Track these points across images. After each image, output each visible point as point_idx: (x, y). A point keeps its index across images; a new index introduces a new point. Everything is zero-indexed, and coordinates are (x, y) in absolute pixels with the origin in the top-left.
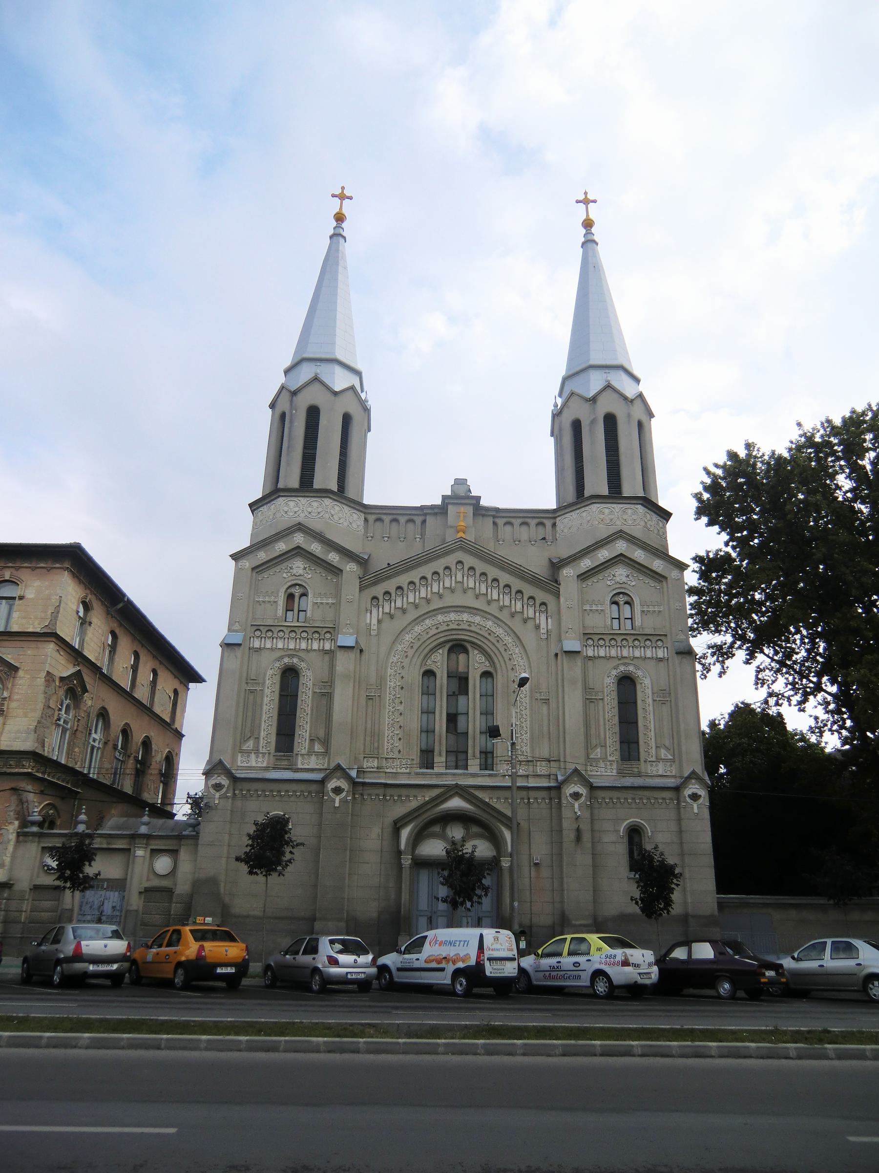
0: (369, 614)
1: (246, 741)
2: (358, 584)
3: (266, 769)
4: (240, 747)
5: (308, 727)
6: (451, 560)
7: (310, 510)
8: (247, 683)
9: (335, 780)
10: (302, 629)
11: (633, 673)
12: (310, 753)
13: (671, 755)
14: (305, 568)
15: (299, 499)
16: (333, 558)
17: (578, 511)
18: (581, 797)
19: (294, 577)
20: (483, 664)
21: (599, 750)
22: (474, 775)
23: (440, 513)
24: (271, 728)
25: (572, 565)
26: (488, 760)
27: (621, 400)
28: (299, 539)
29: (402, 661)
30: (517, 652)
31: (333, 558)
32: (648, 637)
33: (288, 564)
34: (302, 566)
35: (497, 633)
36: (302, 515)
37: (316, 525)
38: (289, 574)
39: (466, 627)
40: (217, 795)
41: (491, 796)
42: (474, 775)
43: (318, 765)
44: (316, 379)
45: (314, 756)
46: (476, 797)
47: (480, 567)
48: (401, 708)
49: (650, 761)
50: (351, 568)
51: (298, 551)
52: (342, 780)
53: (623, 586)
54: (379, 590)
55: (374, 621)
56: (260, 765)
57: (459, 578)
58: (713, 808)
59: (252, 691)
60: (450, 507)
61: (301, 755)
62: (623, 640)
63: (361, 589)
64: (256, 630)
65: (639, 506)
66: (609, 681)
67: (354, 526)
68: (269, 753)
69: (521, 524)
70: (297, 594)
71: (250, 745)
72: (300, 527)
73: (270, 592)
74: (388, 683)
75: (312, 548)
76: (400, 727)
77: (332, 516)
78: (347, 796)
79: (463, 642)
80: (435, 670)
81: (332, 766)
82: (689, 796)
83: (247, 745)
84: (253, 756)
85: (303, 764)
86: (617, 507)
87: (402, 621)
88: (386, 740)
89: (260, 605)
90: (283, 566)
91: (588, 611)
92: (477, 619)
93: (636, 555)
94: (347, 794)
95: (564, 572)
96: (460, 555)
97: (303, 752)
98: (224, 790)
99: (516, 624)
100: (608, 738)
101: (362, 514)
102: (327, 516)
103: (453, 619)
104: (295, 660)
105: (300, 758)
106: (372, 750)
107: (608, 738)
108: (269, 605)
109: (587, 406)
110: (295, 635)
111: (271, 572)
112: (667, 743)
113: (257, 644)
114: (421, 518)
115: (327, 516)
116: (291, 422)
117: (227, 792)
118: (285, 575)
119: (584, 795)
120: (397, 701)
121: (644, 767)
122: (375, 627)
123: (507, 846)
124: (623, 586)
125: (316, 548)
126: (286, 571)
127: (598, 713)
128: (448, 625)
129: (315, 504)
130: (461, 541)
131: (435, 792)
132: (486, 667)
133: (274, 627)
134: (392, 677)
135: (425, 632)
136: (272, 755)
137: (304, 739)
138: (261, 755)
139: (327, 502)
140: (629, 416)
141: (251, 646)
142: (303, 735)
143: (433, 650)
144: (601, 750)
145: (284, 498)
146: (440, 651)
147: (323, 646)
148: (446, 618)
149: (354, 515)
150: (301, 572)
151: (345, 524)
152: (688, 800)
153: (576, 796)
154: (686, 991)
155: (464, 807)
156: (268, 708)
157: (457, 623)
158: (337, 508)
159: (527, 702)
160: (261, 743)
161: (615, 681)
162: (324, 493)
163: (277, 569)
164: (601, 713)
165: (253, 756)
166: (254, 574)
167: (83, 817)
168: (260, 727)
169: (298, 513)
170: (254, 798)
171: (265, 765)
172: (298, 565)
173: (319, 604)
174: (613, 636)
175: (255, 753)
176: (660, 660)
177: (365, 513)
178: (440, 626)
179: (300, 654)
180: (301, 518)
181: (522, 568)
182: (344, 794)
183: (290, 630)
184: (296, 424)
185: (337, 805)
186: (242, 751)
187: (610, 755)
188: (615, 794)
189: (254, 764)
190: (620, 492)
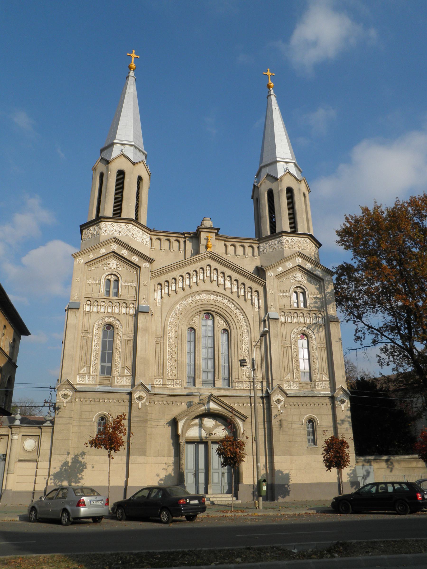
0: (156, 293)
1: (81, 368)
2: (150, 275)
4: (78, 372)
5: (120, 360)
7: (120, 230)
8: (82, 333)
9: (138, 392)
10: (116, 301)
12: (122, 375)
14: (117, 265)
15: (114, 223)
16: (135, 259)
19: (110, 270)
20: (222, 325)
21: (289, 375)
22: (219, 389)
23: (194, 237)
24: (98, 360)
25: (272, 269)
26: (229, 382)
27: (295, 180)
30: (242, 318)
33: (107, 261)
34: (115, 263)
35: (231, 307)
38: (294, 280)
39: (212, 303)
40: (65, 401)
42: (219, 389)
43: (127, 383)
46: (223, 402)
47: (221, 268)
48: (176, 349)
49: (317, 382)
51: (115, 254)
52: (142, 392)
54: (162, 279)
55: (159, 297)
58: (352, 409)
59: (85, 338)
60: (202, 233)
65: (307, 239)
67: (145, 241)
68: (97, 376)
69: (231, 245)
70: (112, 280)
71: (84, 370)
72: (117, 241)
73: (96, 278)
75: (122, 253)
77: (133, 234)
78: (146, 402)
80: (195, 328)
82: (62, 395)
83: (82, 370)
84: (87, 377)
85: (118, 383)
86: (296, 239)
87: (174, 297)
88: (167, 369)
90: (104, 263)
92: (219, 298)
93: (122, 253)
94: (146, 400)
95: (77, 260)
97: (118, 375)
101: (148, 235)
102: (130, 234)
104: (112, 319)
105: (116, 379)
106: (159, 375)
111: (96, 266)
114: (184, 240)
115: (130, 234)
116: (107, 179)
117: (71, 399)
118: (105, 268)
119: (283, 401)
120: (173, 345)
122: (160, 301)
125: (124, 253)
126: (105, 266)
128: (202, 301)
129: (123, 227)
130: (210, 253)
132: (225, 326)
133: (99, 299)
135: (189, 305)
136: (98, 376)
138: (91, 377)
139: (130, 226)
140: (299, 189)
141: (85, 310)
142: (117, 365)
143: (194, 316)
144: (290, 375)
145: (104, 223)
147: (129, 312)
149: (144, 235)
150: (115, 266)
153: (279, 401)
154: (418, 513)
155: (216, 408)
156: (95, 348)
157: (207, 300)
158: (136, 230)
162: (128, 220)
163: (100, 264)
165: (87, 377)
166: (86, 266)
169: (113, 232)
170: (87, 403)
171: (94, 383)
172: (113, 263)
175: (87, 375)
177: (150, 235)
178: (198, 302)
179: (116, 316)
180: (115, 235)
181: (244, 270)
182: (144, 400)
183: (108, 301)
186: (79, 374)
190: (120, 215)
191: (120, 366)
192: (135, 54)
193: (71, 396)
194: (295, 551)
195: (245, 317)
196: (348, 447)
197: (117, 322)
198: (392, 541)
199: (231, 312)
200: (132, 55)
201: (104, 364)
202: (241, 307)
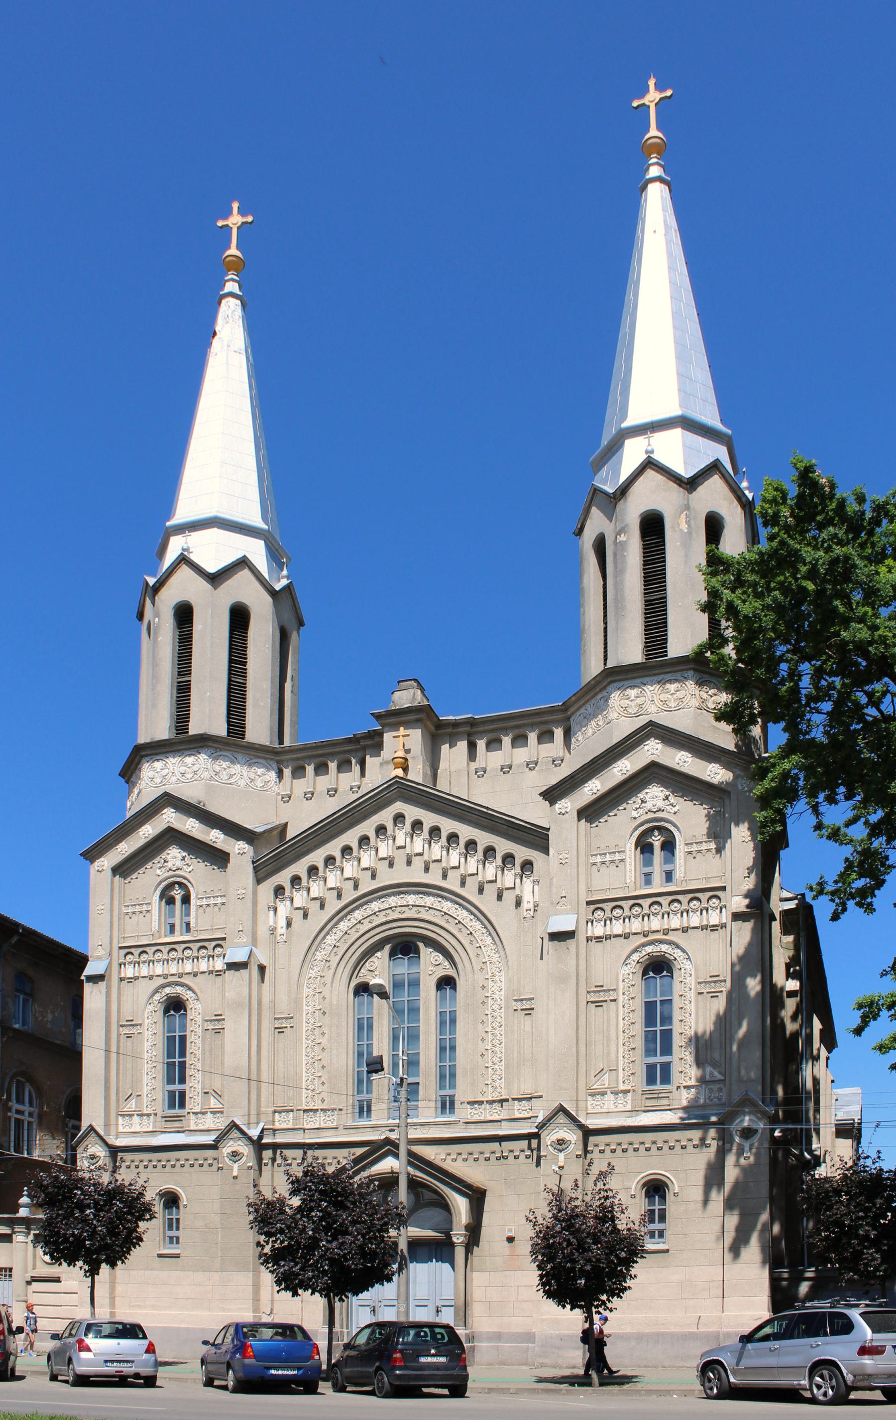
3: (634, 1111)
6: (385, 816)
11: (666, 955)
13: (720, 1073)
16: (216, 837)
17: (593, 701)
18: (753, 1135)
19: (171, 873)
21: (606, 1076)
28: (169, 817)
29: (322, 975)
31: (216, 837)
32: (694, 894)
36: (174, 779)
37: (190, 793)
41: (448, 1152)
44: (650, 464)
45: (209, 1113)
50: (238, 849)
51: (171, 836)
53: (178, 872)
54: (283, 877)
55: (282, 923)
56: (621, 1108)
57: (400, 841)
61: (193, 1113)
62: (186, 948)
63: (259, 881)
64: (186, 948)
66: (628, 971)
74: (305, 1007)
75: (187, 827)
76: (323, 1067)
79: (414, 939)
81: (736, 1098)
85: (197, 1126)
89: (694, 858)
91: (599, 864)
93: (677, 760)
96: (399, 806)
98: (244, 1159)
99: (487, 903)
100: (621, 1058)
103: (393, 904)
107: (621, 1058)
108: (613, 866)
109: (676, 492)
110: (161, 955)
112: (716, 1055)
113: (129, 972)
121: (192, 1123)
123: (461, 1218)
124: (178, 872)
125: (191, 826)
127: (608, 1022)
131: (359, 1151)
134: (310, 999)
137: (196, 1093)
146: (379, 954)
148: (384, 904)
151: (242, 783)
152: (227, 1160)
156: (150, 1055)
159: (502, 1015)
160: (145, 1101)
161: (639, 970)
164: (613, 1022)
167: (24, 1200)
168: (141, 1081)
171: (629, 1107)
172: (174, 855)
173: (617, 862)
174: (172, 947)
176: (714, 928)
184: (160, 639)
185: (235, 1173)
187: (624, 1082)
188: (146, 1156)
189: (612, 1108)
191: (199, 1087)
192: (242, 212)
193: (760, 1131)
194: (675, 1396)
195: (496, 938)
196: (719, 1191)
197: (678, 953)
198: (433, 1355)
199: (460, 930)
200: (646, 100)
201: (172, 1087)
202: (318, 929)
